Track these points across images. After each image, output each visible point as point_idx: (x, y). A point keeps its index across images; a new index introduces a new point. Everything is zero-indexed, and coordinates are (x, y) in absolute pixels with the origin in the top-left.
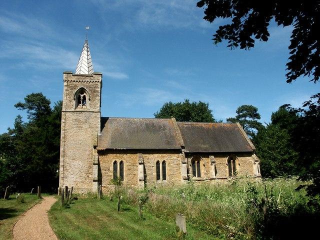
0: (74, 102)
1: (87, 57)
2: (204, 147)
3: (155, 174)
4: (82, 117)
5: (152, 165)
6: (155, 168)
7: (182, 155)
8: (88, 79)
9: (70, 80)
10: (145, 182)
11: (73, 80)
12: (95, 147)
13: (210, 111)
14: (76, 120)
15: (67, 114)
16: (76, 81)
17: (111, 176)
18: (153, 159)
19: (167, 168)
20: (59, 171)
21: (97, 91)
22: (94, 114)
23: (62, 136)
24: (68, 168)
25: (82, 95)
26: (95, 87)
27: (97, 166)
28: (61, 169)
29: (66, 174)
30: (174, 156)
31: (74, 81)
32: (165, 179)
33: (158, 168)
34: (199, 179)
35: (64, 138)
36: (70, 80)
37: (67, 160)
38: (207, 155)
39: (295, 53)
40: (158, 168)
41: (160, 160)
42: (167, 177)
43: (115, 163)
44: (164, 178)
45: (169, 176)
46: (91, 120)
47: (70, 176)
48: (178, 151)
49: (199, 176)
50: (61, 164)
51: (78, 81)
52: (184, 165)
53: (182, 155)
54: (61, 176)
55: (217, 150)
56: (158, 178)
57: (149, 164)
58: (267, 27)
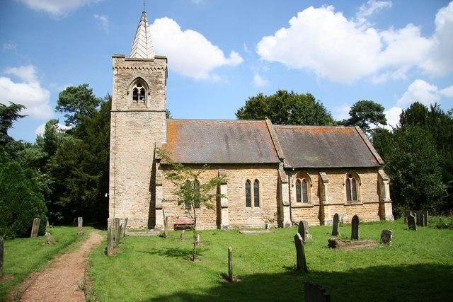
0: (130, 97)
1: (144, 35)
2: (311, 160)
4: (138, 119)
6: (243, 191)
8: (147, 65)
9: (122, 67)
11: (126, 67)
14: (131, 122)
15: (119, 115)
16: (130, 68)
18: (238, 178)
19: (261, 190)
20: (108, 196)
21: (161, 83)
22: (156, 115)
24: (120, 190)
25: (139, 88)
27: (327, 203)
28: (111, 192)
29: (119, 198)
30: (272, 173)
31: (128, 68)
33: (248, 189)
35: (115, 148)
36: (122, 67)
37: (119, 179)
38: (317, 171)
42: (261, 203)
44: (257, 204)
46: (152, 123)
47: (125, 202)
48: (274, 166)
49: (306, 200)
50: (111, 185)
51: (134, 68)
54: (111, 201)
56: (249, 204)
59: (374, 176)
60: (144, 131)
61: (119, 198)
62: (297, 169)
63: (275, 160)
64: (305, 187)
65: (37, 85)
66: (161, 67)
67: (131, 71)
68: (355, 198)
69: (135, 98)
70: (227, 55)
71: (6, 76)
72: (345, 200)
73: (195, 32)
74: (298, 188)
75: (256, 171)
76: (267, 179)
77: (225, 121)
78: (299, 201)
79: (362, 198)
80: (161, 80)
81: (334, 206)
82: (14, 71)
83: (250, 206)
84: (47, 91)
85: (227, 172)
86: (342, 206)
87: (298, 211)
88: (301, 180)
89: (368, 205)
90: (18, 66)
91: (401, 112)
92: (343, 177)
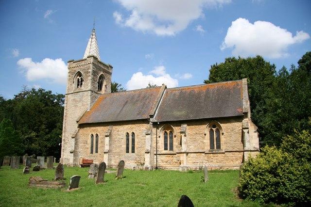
0: (75, 85)
3: (125, 146)
5: (121, 137)
6: (124, 141)
7: (150, 125)
8: (83, 63)
10: (76, 140)
12: (77, 122)
13: (40, 91)
14: (74, 100)
15: (69, 96)
17: (88, 148)
18: (121, 131)
19: (136, 140)
22: (86, 93)
23: (65, 114)
26: (88, 69)
29: (66, 146)
30: (144, 127)
32: (128, 152)
33: (128, 140)
34: (171, 152)
38: (179, 123)
39: (161, 32)
40: (128, 140)
41: (129, 132)
43: (92, 135)
44: (133, 151)
45: (137, 148)
47: (299, 123)
48: (146, 121)
49: (171, 149)
52: (148, 136)
53: (150, 125)
54: (62, 148)
55: (192, 117)
56: (128, 151)
57: (118, 137)
58: (61, 59)
59: (237, 126)
60: (80, 104)
61: (66, 146)
62: (162, 123)
63: (145, 117)
64: (171, 138)
65: (168, 76)
66: (90, 63)
67: (74, 69)
68: (219, 147)
69: (78, 85)
70: (294, 35)
71: (150, 74)
72: (207, 148)
73: (264, 22)
74: (166, 138)
75: (133, 126)
76: (140, 130)
77: (134, 91)
78: (166, 149)
79: (223, 147)
80: (89, 70)
81: (195, 154)
82: (153, 71)
83: (128, 152)
84: (176, 80)
85: (115, 128)
86: (203, 154)
87: (164, 158)
88: (168, 132)
89: (231, 153)
90: (154, 69)
91: (210, 68)
92: (205, 129)
